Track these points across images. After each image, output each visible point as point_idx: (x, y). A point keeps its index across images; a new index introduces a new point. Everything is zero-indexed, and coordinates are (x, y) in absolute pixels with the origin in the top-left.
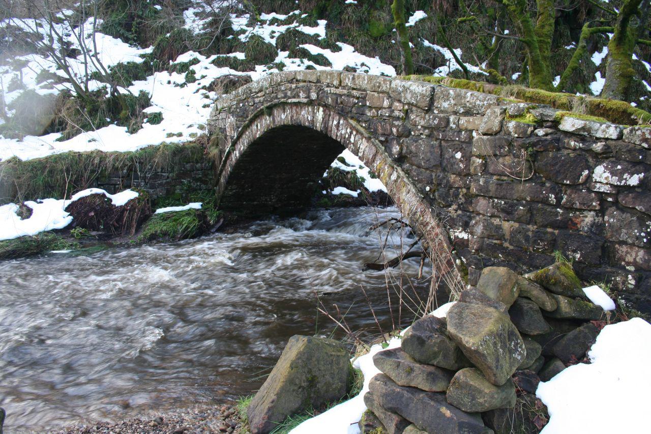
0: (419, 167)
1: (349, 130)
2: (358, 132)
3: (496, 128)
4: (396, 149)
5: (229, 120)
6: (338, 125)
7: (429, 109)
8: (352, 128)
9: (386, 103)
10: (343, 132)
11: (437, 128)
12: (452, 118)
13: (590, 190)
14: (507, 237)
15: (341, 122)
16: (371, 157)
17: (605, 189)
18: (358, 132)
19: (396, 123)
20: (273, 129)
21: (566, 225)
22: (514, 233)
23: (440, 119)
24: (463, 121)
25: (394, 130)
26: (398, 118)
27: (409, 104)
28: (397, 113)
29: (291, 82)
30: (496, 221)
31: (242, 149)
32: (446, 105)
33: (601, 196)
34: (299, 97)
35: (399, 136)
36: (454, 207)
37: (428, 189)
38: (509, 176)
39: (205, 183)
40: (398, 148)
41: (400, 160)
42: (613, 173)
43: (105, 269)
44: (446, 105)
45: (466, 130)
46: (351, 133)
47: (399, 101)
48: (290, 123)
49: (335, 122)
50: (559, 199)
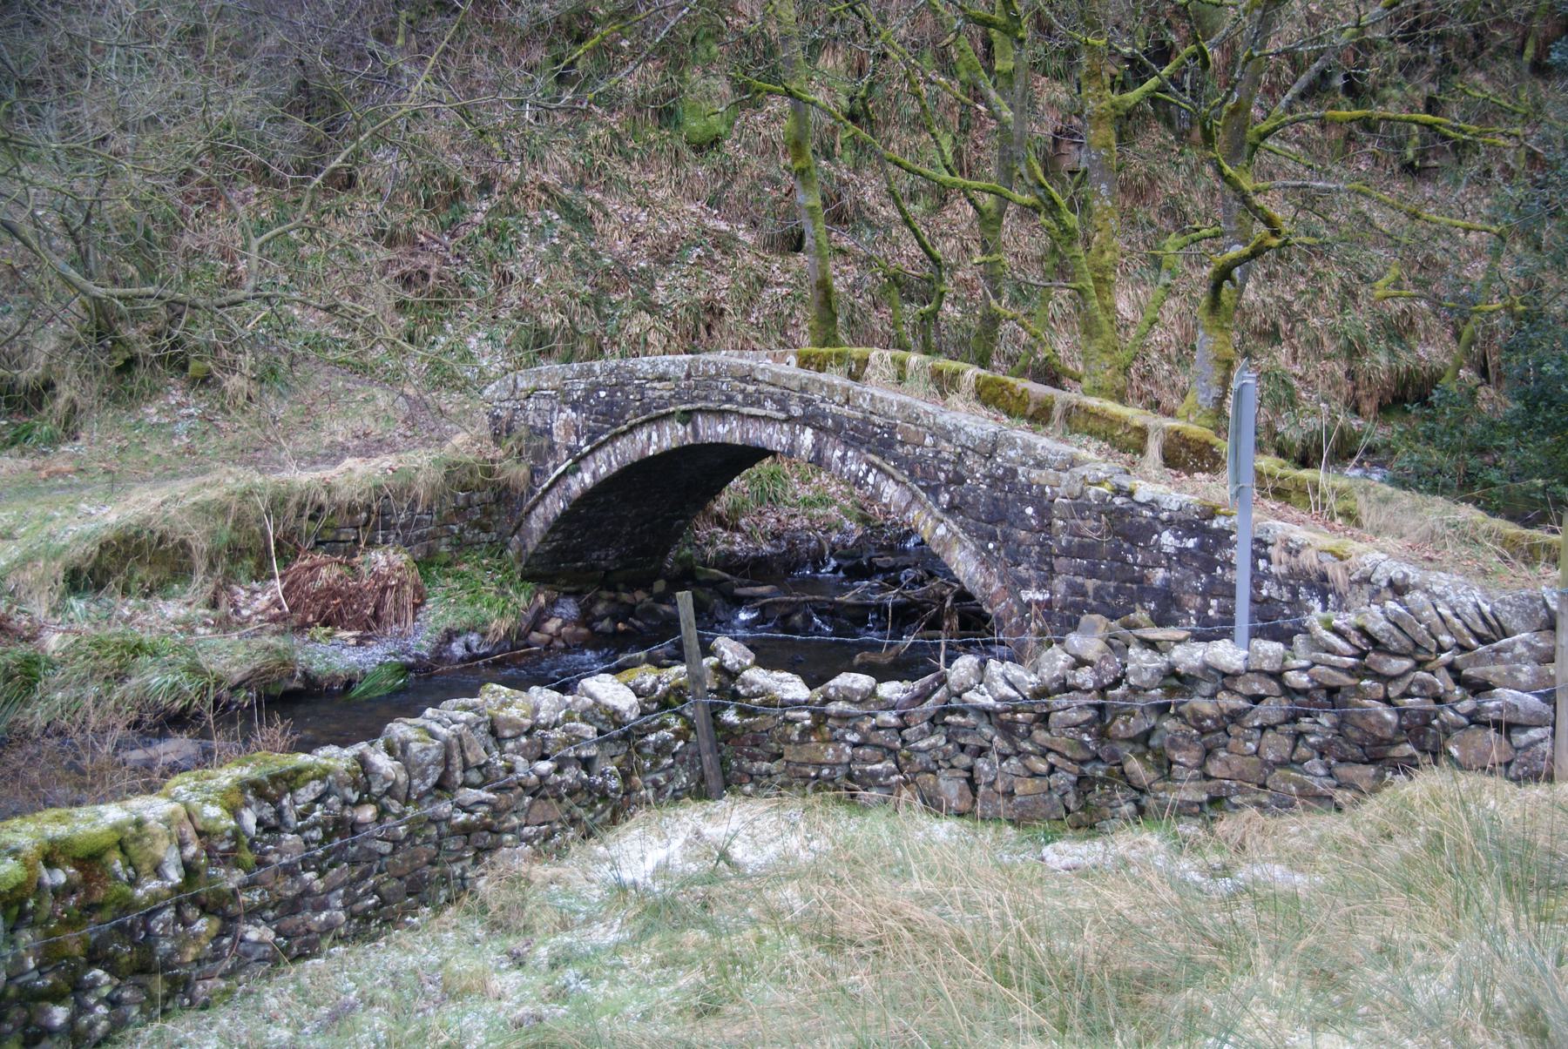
0: (978, 519)
1: (864, 467)
2: (880, 469)
3: (1077, 493)
4: (945, 498)
5: (563, 416)
6: (843, 459)
7: (991, 456)
8: (871, 465)
9: (929, 441)
10: (853, 468)
11: (1002, 479)
12: (1020, 470)
13: (1159, 550)
14: (1091, 593)
15: (850, 454)
16: (903, 504)
17: (1170, 550)
18: (880, 469)
19: (945, 467)
20: (690, 447)
21: (1140, 580)
22: (1097, 590)
23: (1006, 470)
24: (1035, 474)
25: (942, 476)
26: (947, 461)
27: (962, 446)
28: (945, 455)
29: (743, 379)
30: (1079, 580)
31: (603, 470)
32: (1012, 454)
33: (1168, 557)
34: (763, 407)
35: (949, 482)
36: (1025, 565)
37: (991, 546)
38: (27, 244)
39: (485, 529)
40: (947, 497)
41: (951, 509)
42: (1176, 537)
43: (853, 709)
44: (1012, 454)
45: (1039, 485)
46: (869, 471)
47: (949, 441)
48: (738, 442)
49: (838, 453)
50: (1135, 559)
